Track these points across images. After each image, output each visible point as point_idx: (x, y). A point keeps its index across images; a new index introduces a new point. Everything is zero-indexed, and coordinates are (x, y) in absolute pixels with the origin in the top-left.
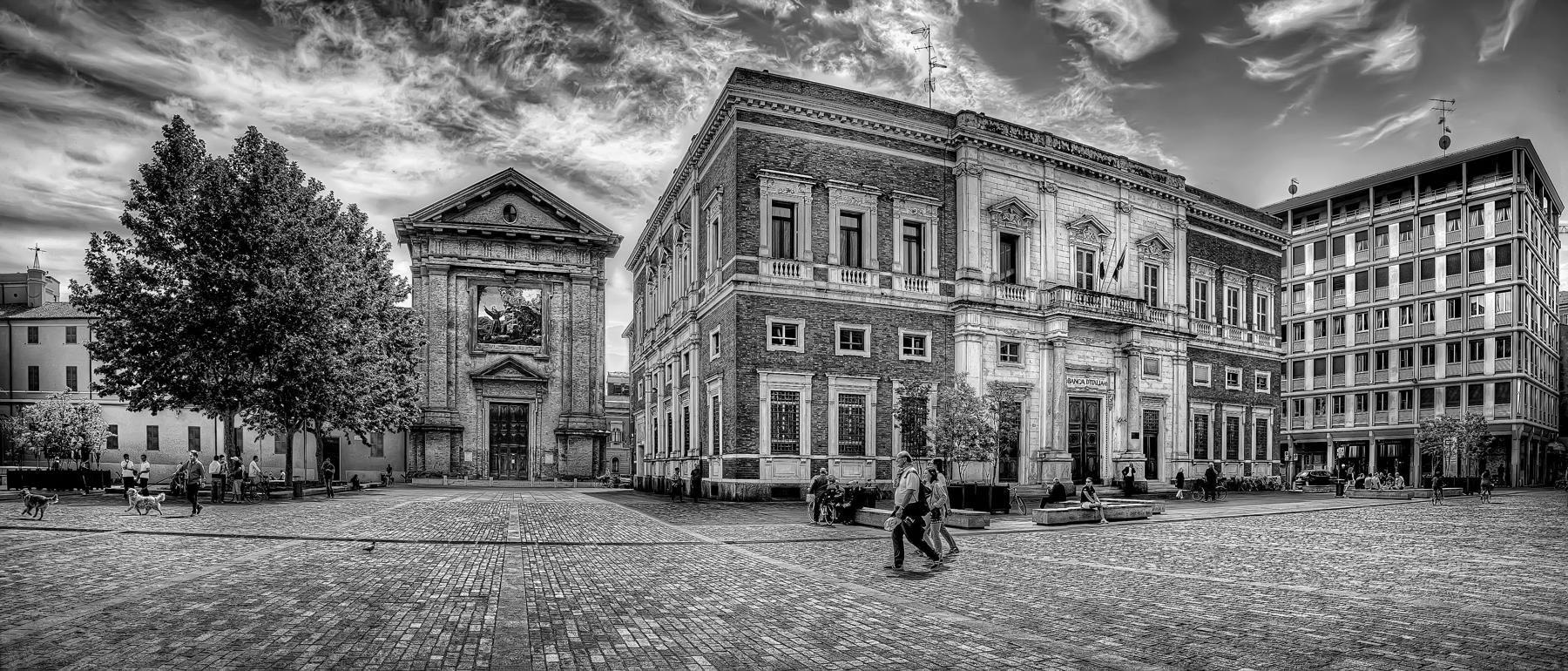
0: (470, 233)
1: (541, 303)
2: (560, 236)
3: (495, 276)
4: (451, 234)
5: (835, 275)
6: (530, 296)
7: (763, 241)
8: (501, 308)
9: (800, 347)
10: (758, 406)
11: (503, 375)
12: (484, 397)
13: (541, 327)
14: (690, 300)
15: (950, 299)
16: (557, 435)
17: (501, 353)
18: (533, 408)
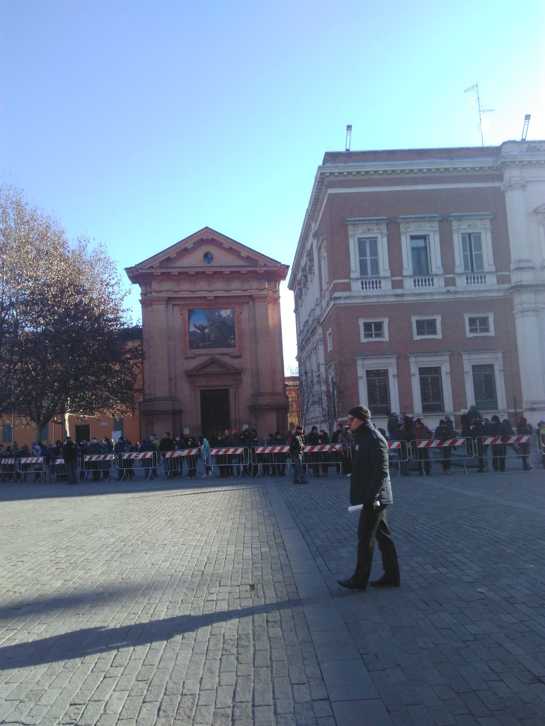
0: (180, 273)
1: (233, 317)
2: (244, 270)
3: (200, 302)
4: (166, 276)
5: (409, 284)
6: (225, 313)
7: (353, 267)
8: (204, 323)
9: (386, 338)
10: (357, 383)
11: (209, 370)
12: (196, 387)
13: (234, 334)
14: (316, 311)
15: (507, 286)
16: (250, 410)
17: (207, 355)
18: (232, 391)
